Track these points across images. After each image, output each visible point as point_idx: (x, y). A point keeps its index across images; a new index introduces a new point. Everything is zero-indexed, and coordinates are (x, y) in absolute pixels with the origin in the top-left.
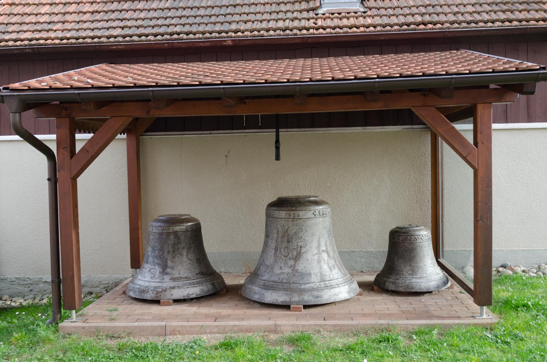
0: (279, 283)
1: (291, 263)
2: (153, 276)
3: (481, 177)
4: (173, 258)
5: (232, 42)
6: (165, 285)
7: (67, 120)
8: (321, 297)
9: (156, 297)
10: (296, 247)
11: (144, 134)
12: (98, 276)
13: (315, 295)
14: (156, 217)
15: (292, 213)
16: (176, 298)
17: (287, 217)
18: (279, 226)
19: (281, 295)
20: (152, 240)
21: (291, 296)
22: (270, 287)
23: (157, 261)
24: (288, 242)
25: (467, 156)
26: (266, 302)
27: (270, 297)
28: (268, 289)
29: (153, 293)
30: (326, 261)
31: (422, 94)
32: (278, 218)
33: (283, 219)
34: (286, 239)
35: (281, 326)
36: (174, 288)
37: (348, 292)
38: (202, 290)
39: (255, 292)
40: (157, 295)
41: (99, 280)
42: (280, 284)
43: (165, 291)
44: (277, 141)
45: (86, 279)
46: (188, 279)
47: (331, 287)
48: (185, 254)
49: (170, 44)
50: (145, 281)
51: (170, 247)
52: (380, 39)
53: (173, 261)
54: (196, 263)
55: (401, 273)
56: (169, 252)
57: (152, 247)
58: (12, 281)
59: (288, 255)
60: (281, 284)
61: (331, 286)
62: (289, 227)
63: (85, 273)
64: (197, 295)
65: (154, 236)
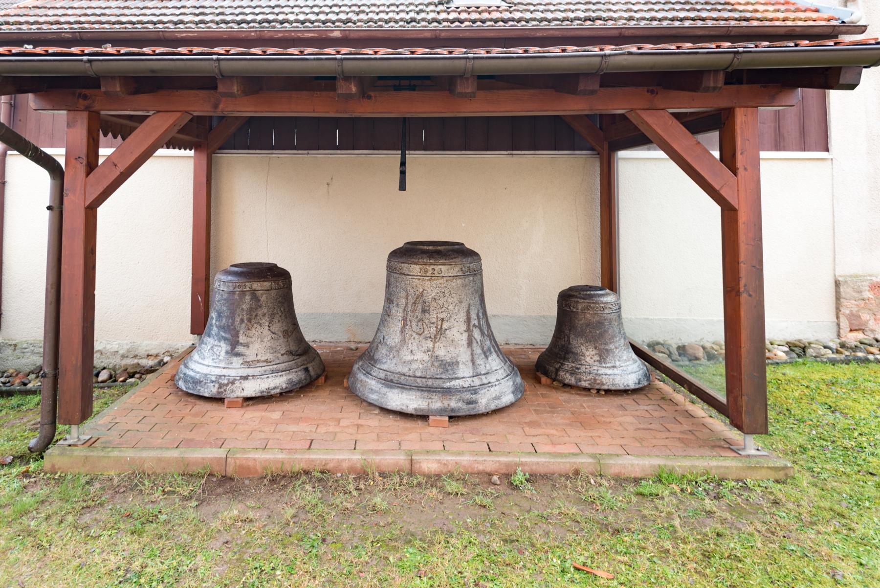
0: (409, 376)
1: (428, 345)
2: (216, 358)
3: (744, 223)
4: (249, 329)
5: (341, 33)
6: (233, 373)
7: (85, 115)
8: (477, 403)
9: (219, 393)
10: (434, 320)
11: (218, 151)
12: (145, 342)
13: (468, 399)
14: (227, 266)
15: (430, 268)
16: (249, 396)
17: (422, 273)
18: (409, 288)
19: (414, 397)
20: (218, 301)
21: (430, 401)
22: (396, 382)
23: (224, 334)
24: (424, 311)
25: (720, 189)
26: (389, 408)
27: (397, 400)
28: (391, 387)
29: (214, 386)
30: (479, 343)
31: (648, 91)
32: (408, 275)
33: (415, 277)
34: (420, 307)
35: (420, 462)
36: (247, 379)
37: (513, 392)
38: (290, 381)
39: (372, 390)
40: (220, 390)
41: (145, 348)
42: (411, 378)
43: (233, 383)
44: (403, 164)
45: (128, 347)
46: (269, 364)
47: (490, 385)
48: (267, 324)
49: (258, 33)
50: (203, 365)
51: (245, 313)
52: (535, 36)
53: (247, 334)
54: (282, 337)
55: (583, 358)
56: (242, 321)
57: (217, 311)
58: (24, 348)
59: (423, 332)
60: (413, 379)
61: (490, 383)
62: (424, 290)
63: (128, 338)
64: (282, 389)
65: (222, 295)
